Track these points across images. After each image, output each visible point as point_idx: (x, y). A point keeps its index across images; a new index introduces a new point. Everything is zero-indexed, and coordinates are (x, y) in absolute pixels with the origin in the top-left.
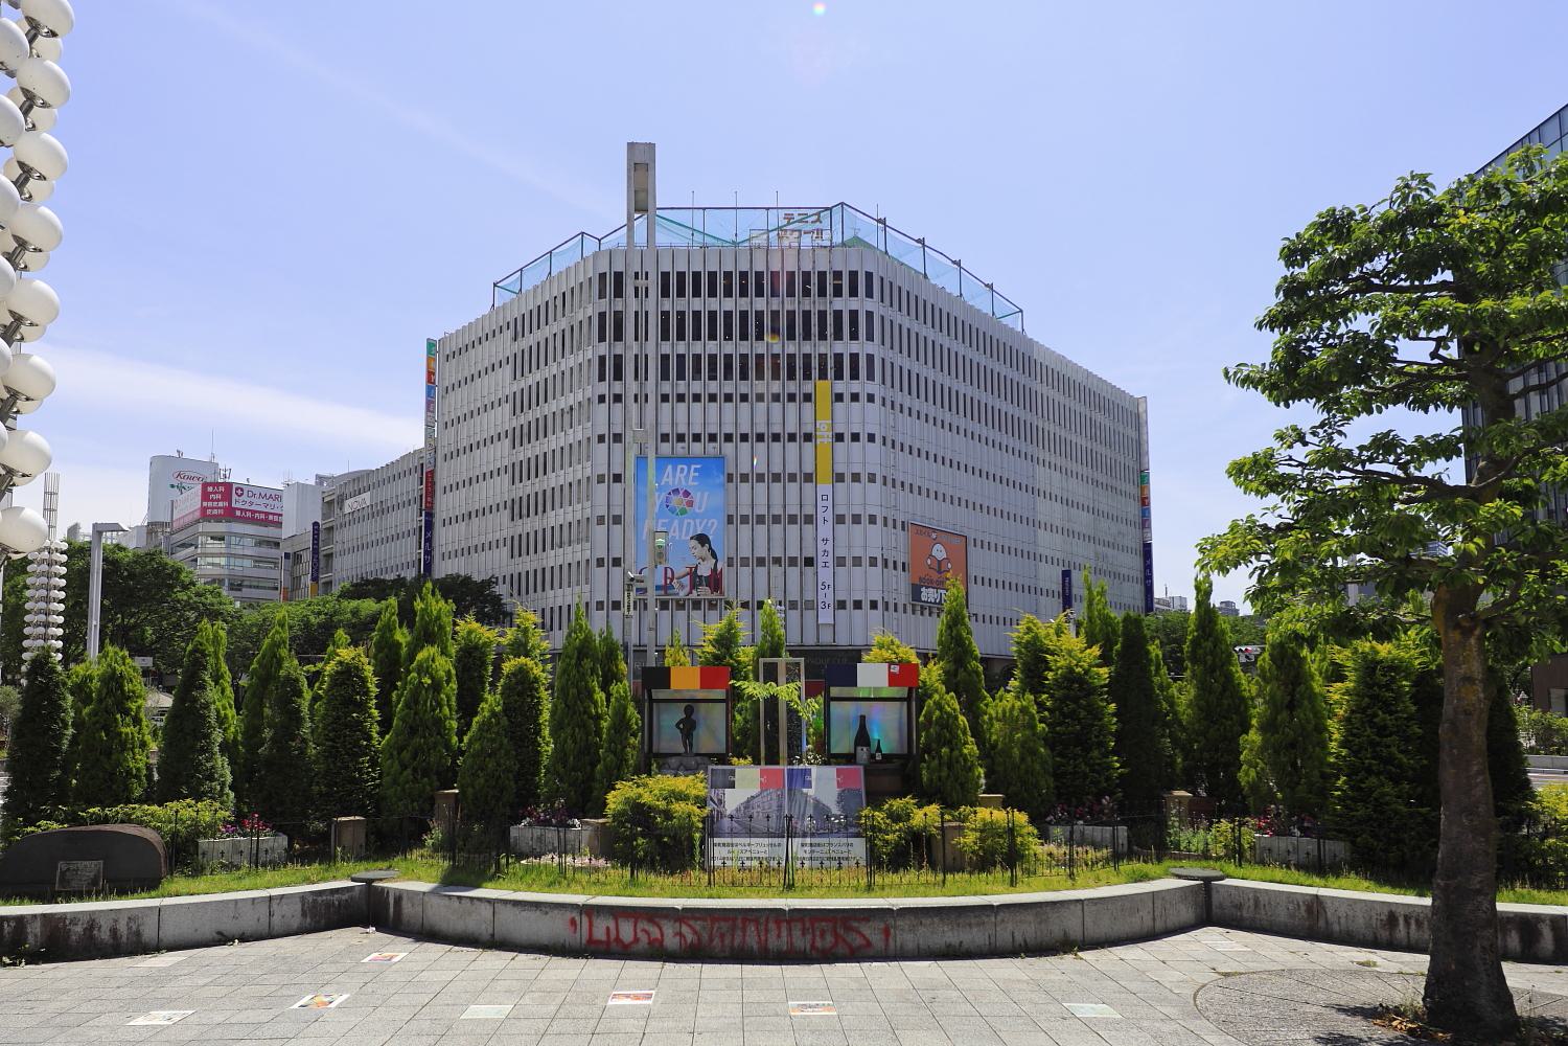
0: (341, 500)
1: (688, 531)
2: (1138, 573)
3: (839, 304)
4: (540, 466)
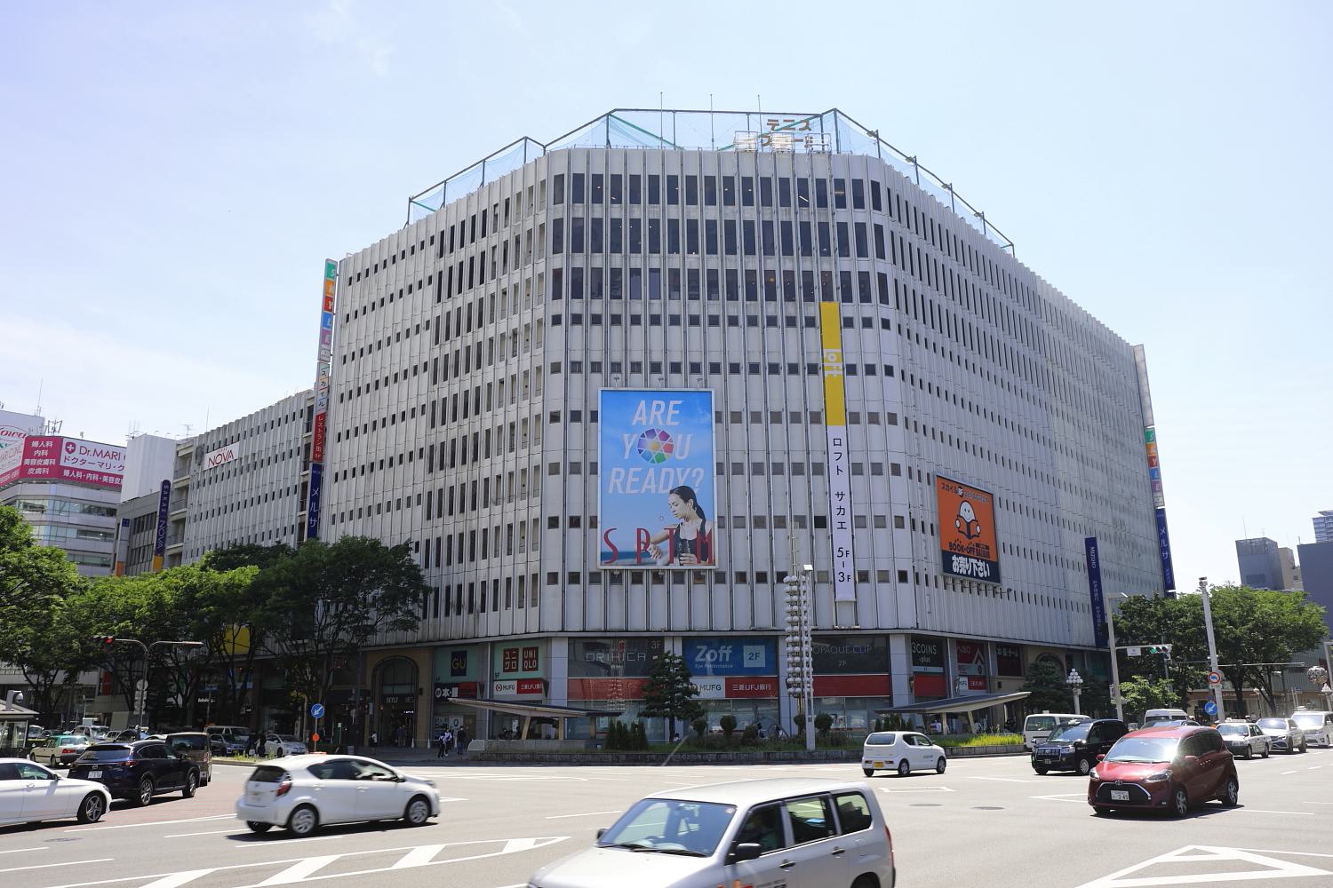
0: (201, 454)
1: (667, 482)
2: (1153, 544)
3: (843, 215)
4: (472, 404)
